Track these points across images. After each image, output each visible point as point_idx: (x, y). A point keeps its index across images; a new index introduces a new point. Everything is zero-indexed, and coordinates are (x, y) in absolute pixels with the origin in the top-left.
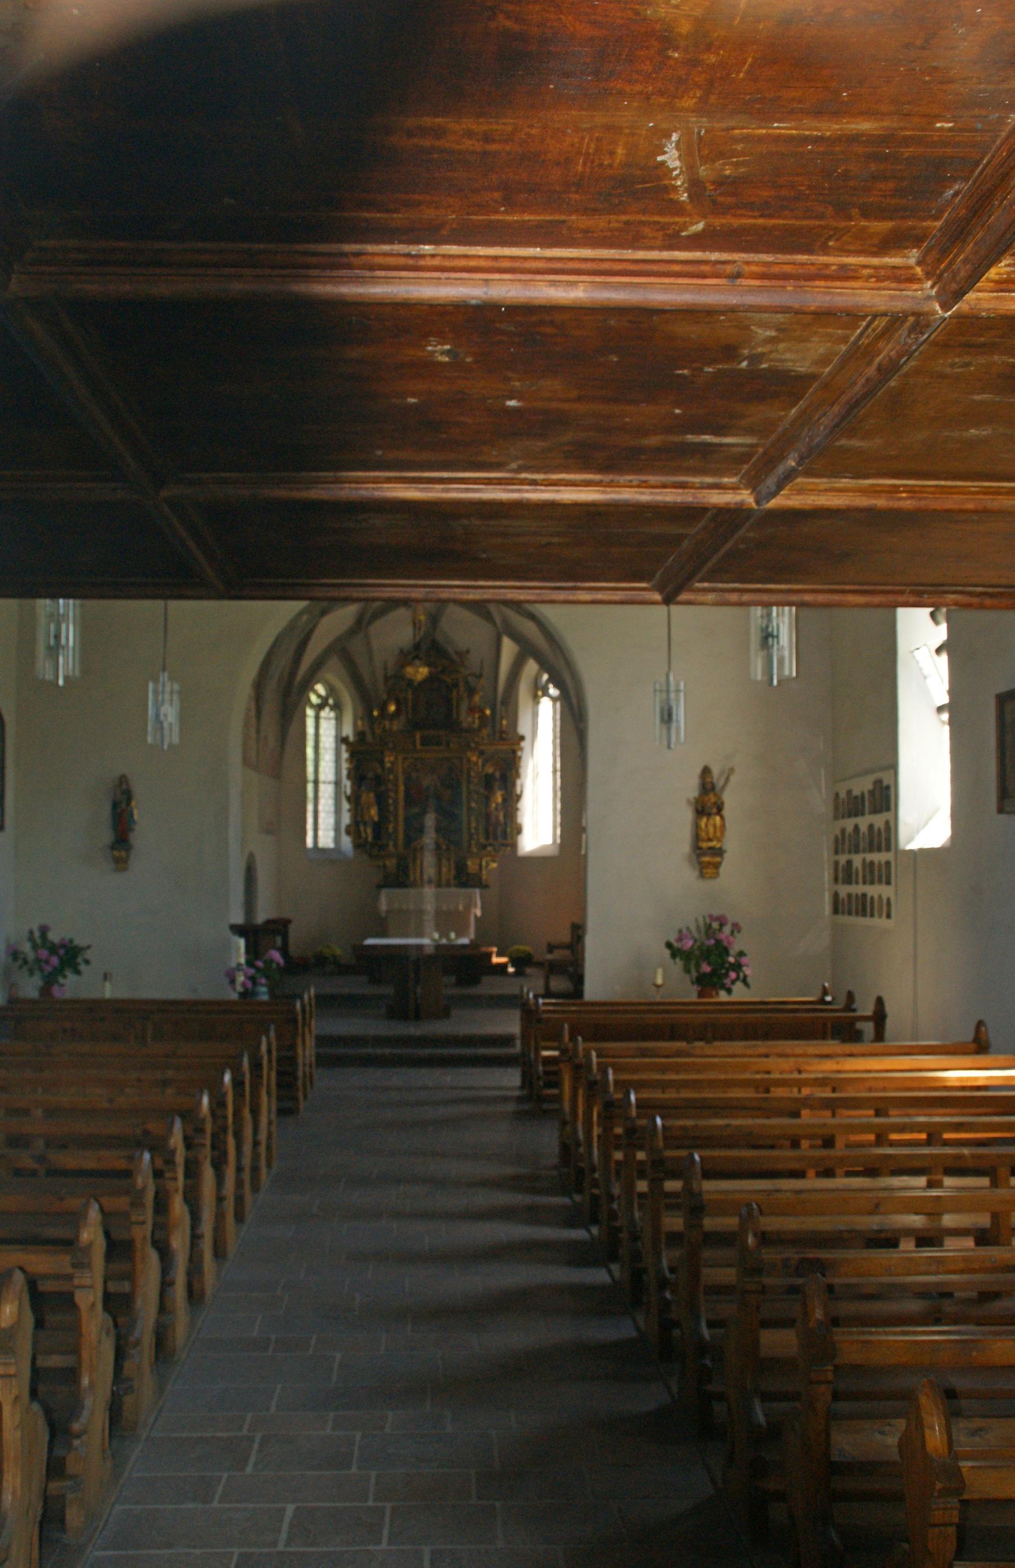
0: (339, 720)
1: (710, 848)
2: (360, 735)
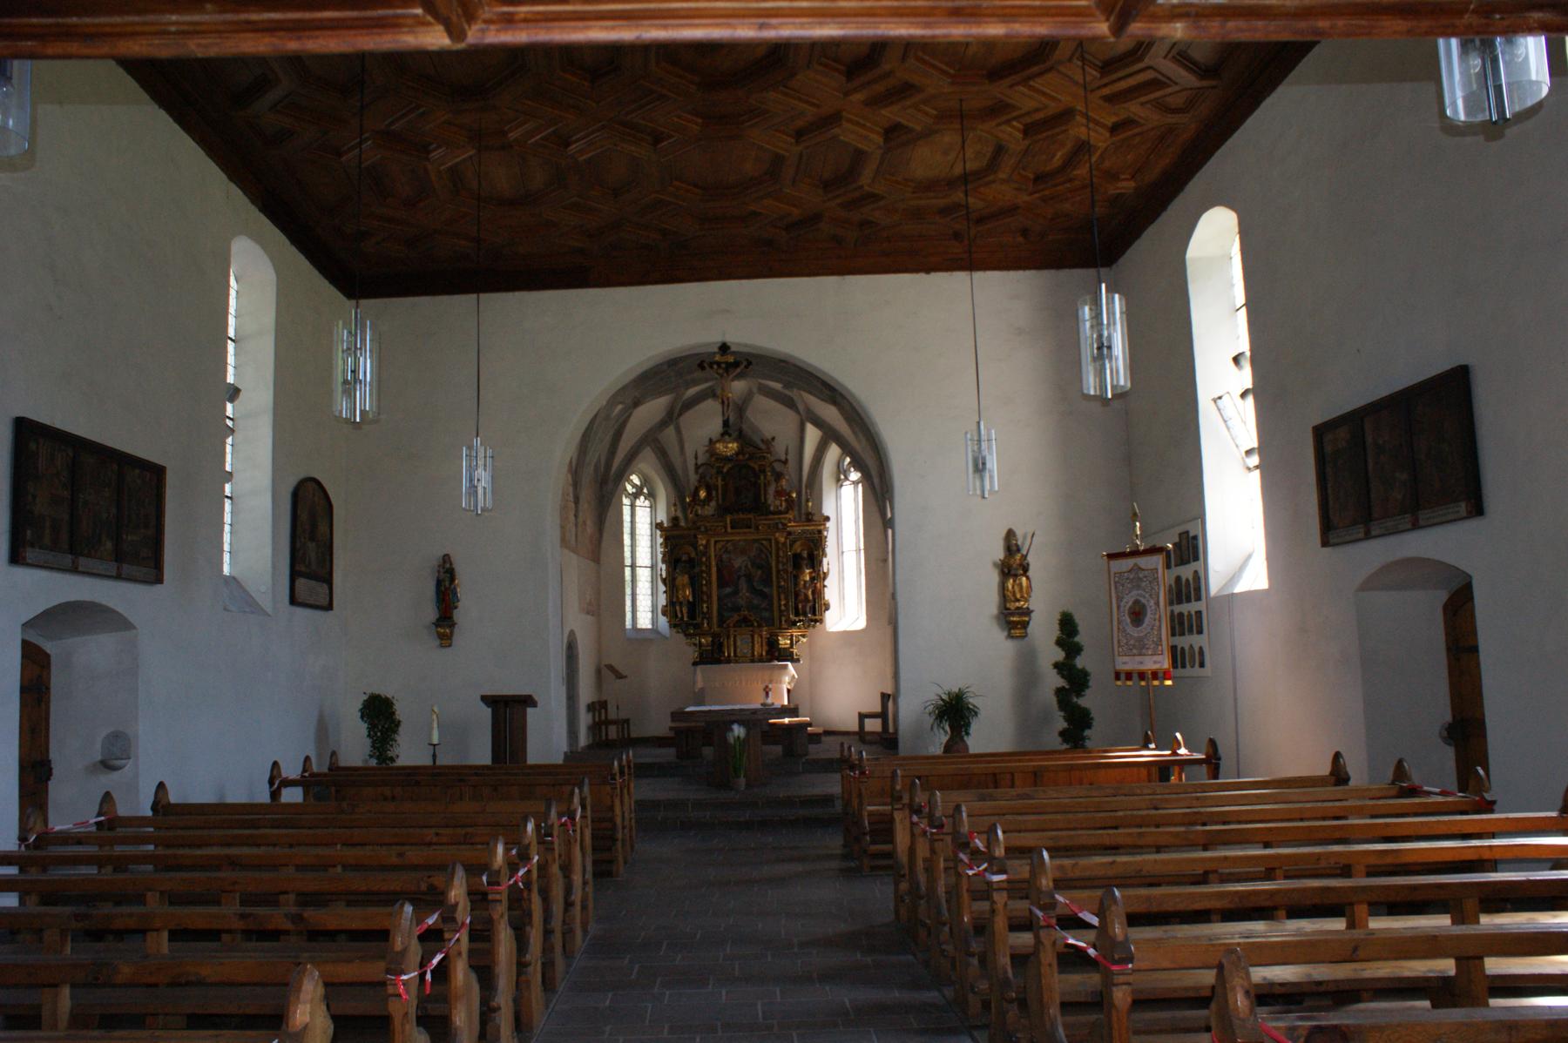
0: (653, 508)
2: (674, 520)
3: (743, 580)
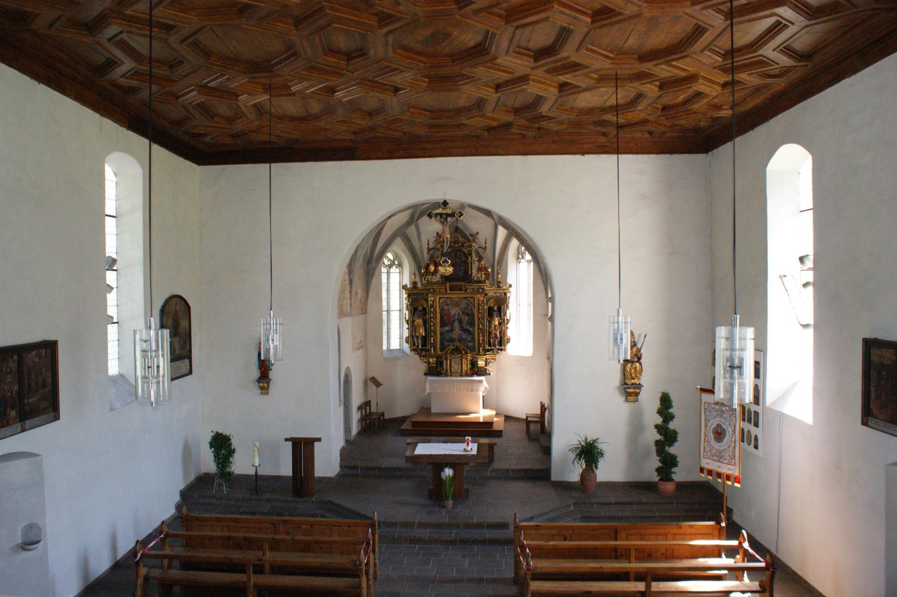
1: (633, 384)
3: (457, 322)
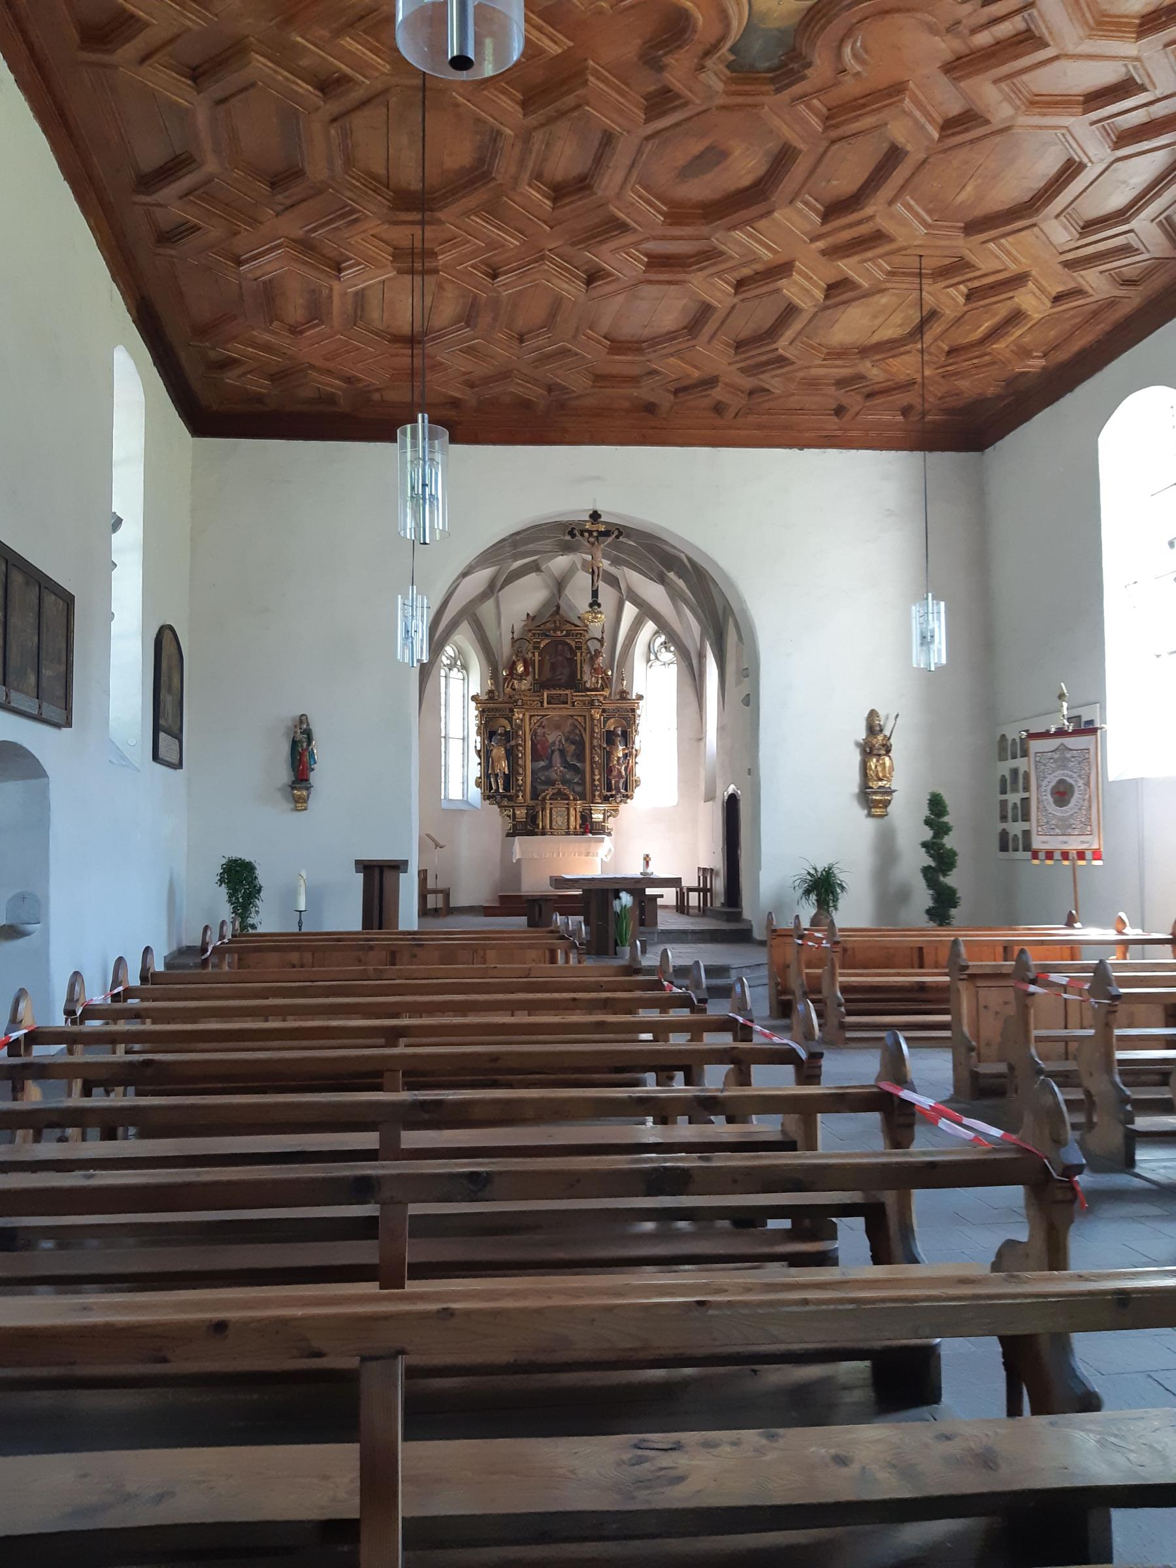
1: (880, 787)
3: (557, 754)
